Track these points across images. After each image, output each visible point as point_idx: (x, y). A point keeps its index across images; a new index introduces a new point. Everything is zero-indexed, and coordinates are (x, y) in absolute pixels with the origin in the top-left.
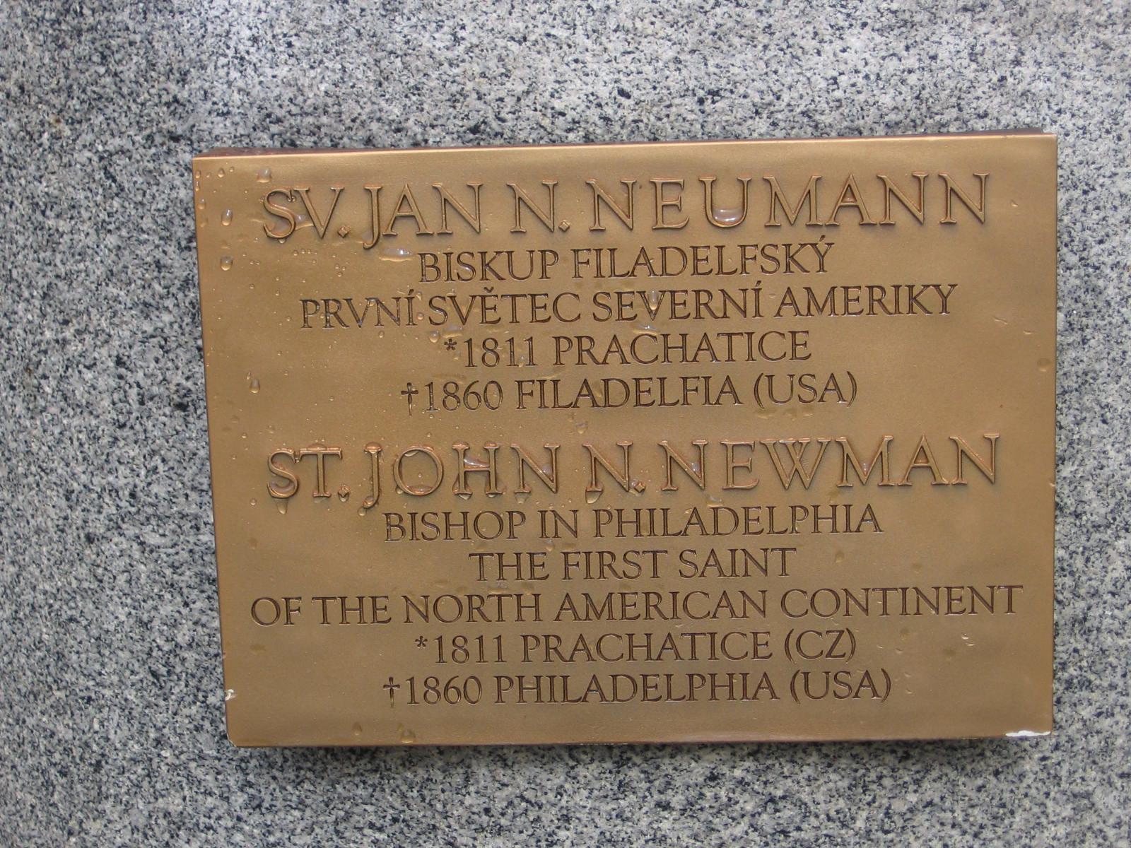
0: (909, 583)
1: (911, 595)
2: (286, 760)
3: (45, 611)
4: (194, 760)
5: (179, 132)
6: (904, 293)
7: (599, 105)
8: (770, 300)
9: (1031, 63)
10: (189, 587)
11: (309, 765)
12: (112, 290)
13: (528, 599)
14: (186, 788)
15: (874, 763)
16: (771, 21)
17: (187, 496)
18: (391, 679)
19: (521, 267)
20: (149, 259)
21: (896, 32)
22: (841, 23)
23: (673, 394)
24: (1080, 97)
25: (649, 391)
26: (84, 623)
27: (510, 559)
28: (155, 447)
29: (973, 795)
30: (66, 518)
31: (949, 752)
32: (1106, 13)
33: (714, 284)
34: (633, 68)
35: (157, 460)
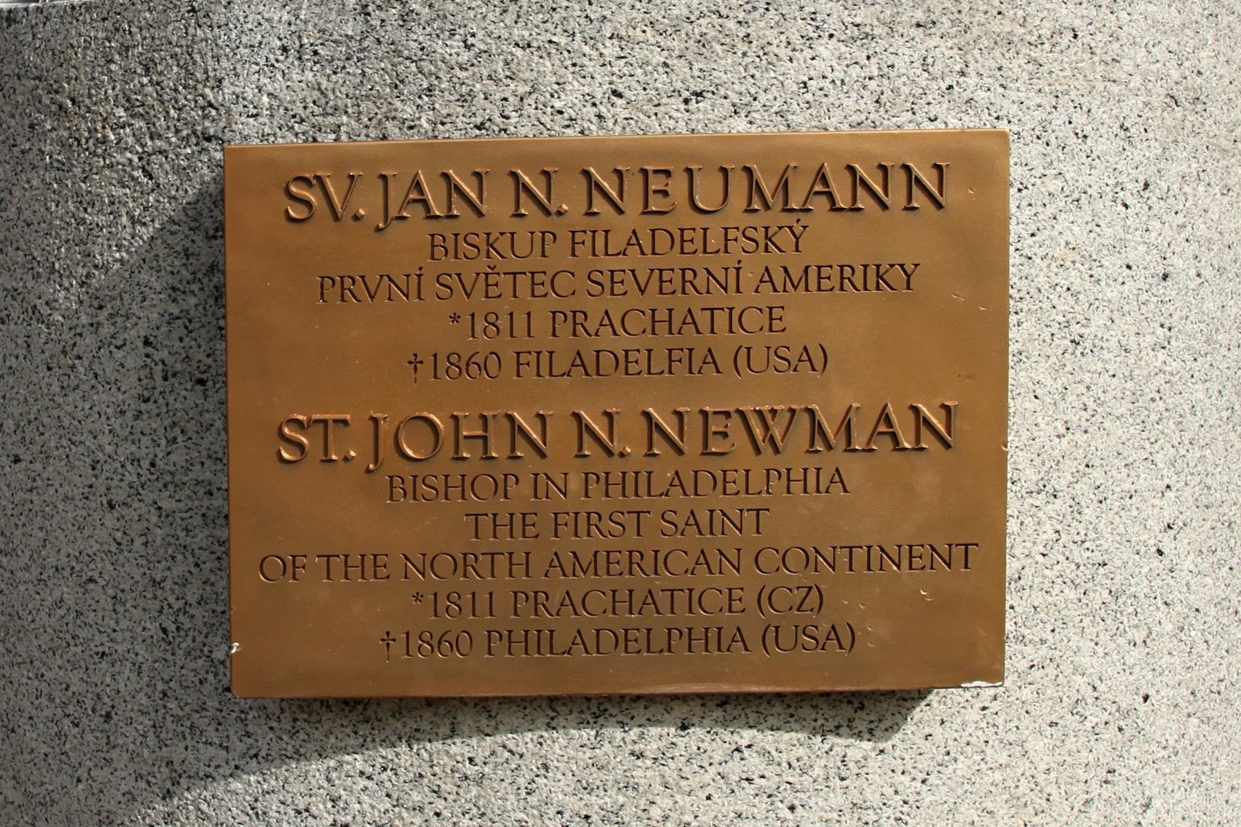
0: (873, 540)
1: (875, 551)
2: (282, 711)
3: (67, 573)
4: (197, 711)
5: (212, 132)
6: (872, 270)
7: (594, 105)
8: (750, 277)
9: (973, 74)
10: (200, 548)
11: (305, 716)
12: (144, 277)
13: (520, 557)
14: (188, 737)
15: (832, 713)
16: (749, 31)
17: (203, 463)
18: (388, 633)
19: (522, 246)
20: (178, 248)
21: (859, 43)
22: (811, 35)
23: (660, 363)
24: (1016, 106)
25: (692, 241)
26: (102, 583)
27: (503, 519)
28: (176, 419)
29: (921, 742)
30: (91, 486)
31: (901, 702)
32: (1036, 33)
33: (700, 262)
34: (625, 70)
35: (177, 431)
